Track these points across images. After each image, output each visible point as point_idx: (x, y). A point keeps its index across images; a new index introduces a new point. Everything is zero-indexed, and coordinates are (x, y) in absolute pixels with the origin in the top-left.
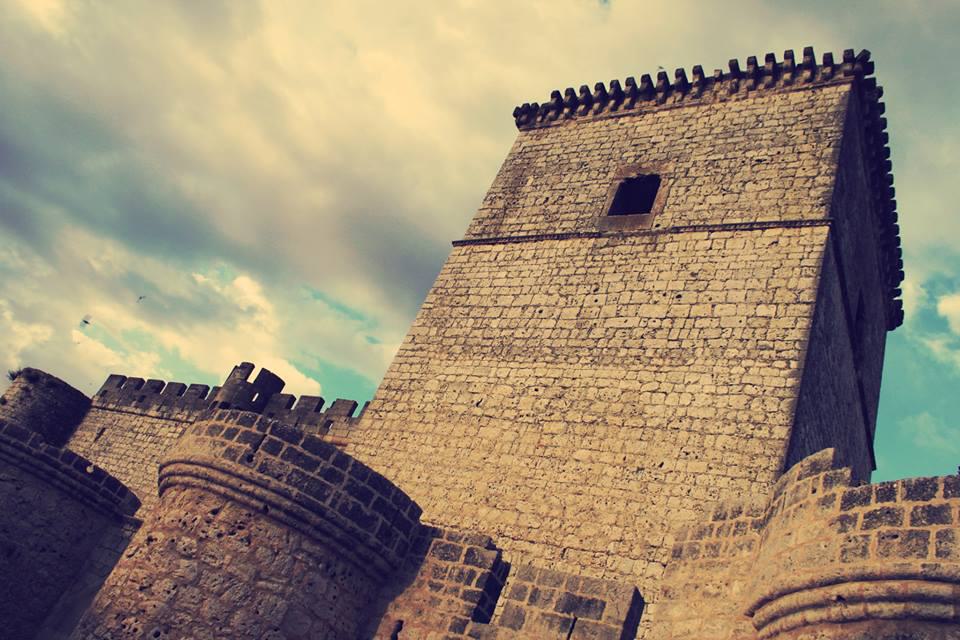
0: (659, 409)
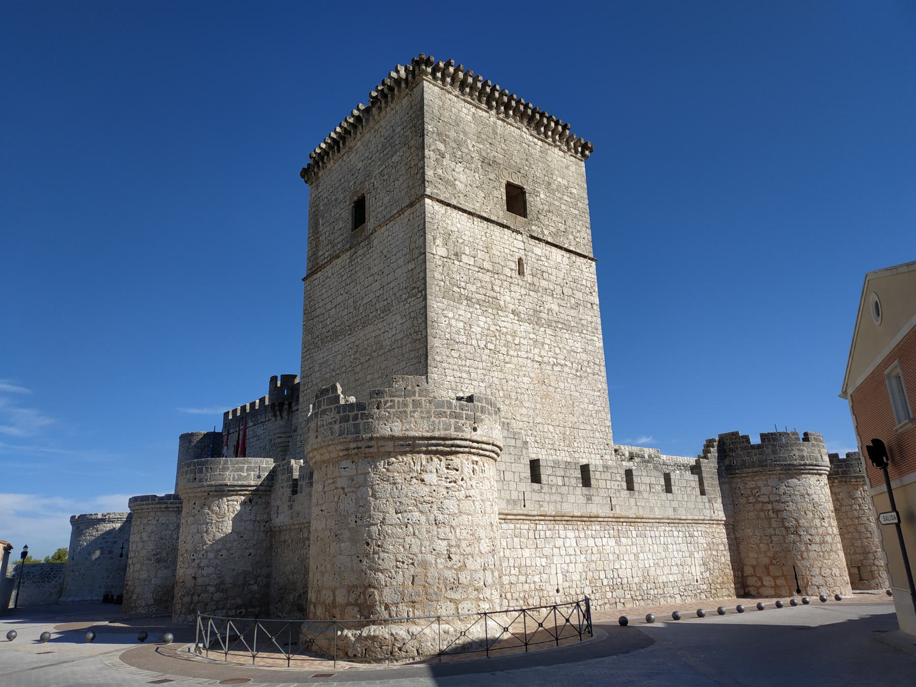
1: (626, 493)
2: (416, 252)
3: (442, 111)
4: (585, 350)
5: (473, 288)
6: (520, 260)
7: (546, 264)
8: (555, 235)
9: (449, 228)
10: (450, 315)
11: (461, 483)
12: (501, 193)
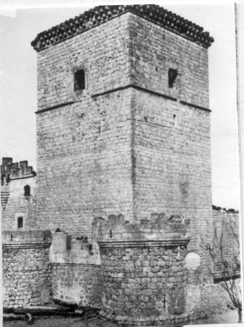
0: (103, 163)
5: (153, 137)
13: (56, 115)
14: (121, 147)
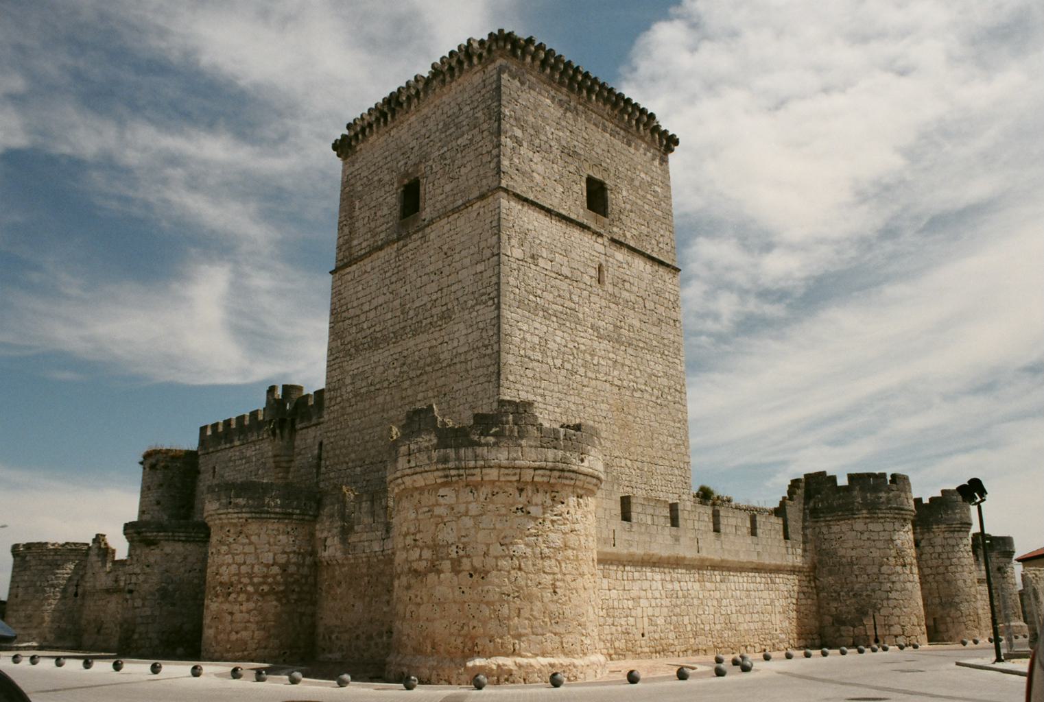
0: (446, 354)
1: (712, 535)
2: (487, 253)
3: (519, 93)
4: (665, 373)
5: (550, 297)
6: (600, 266)
7: (628, 272)
8: (638, 238)
9: (526, 226)
10: (525, 327)
11: (567, 516)
12: (581, 188)
13: (366, 272)
14: (480, 312)
